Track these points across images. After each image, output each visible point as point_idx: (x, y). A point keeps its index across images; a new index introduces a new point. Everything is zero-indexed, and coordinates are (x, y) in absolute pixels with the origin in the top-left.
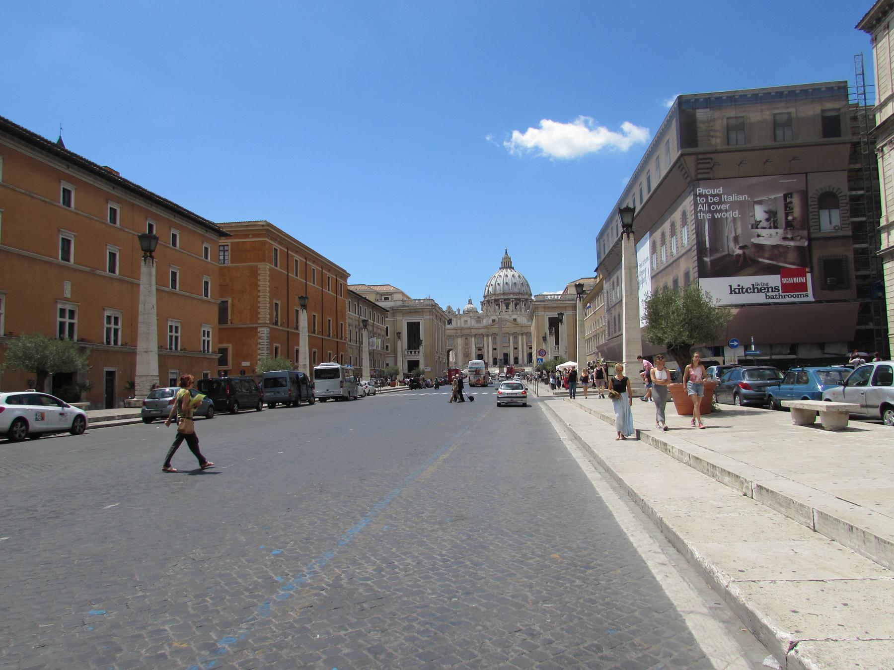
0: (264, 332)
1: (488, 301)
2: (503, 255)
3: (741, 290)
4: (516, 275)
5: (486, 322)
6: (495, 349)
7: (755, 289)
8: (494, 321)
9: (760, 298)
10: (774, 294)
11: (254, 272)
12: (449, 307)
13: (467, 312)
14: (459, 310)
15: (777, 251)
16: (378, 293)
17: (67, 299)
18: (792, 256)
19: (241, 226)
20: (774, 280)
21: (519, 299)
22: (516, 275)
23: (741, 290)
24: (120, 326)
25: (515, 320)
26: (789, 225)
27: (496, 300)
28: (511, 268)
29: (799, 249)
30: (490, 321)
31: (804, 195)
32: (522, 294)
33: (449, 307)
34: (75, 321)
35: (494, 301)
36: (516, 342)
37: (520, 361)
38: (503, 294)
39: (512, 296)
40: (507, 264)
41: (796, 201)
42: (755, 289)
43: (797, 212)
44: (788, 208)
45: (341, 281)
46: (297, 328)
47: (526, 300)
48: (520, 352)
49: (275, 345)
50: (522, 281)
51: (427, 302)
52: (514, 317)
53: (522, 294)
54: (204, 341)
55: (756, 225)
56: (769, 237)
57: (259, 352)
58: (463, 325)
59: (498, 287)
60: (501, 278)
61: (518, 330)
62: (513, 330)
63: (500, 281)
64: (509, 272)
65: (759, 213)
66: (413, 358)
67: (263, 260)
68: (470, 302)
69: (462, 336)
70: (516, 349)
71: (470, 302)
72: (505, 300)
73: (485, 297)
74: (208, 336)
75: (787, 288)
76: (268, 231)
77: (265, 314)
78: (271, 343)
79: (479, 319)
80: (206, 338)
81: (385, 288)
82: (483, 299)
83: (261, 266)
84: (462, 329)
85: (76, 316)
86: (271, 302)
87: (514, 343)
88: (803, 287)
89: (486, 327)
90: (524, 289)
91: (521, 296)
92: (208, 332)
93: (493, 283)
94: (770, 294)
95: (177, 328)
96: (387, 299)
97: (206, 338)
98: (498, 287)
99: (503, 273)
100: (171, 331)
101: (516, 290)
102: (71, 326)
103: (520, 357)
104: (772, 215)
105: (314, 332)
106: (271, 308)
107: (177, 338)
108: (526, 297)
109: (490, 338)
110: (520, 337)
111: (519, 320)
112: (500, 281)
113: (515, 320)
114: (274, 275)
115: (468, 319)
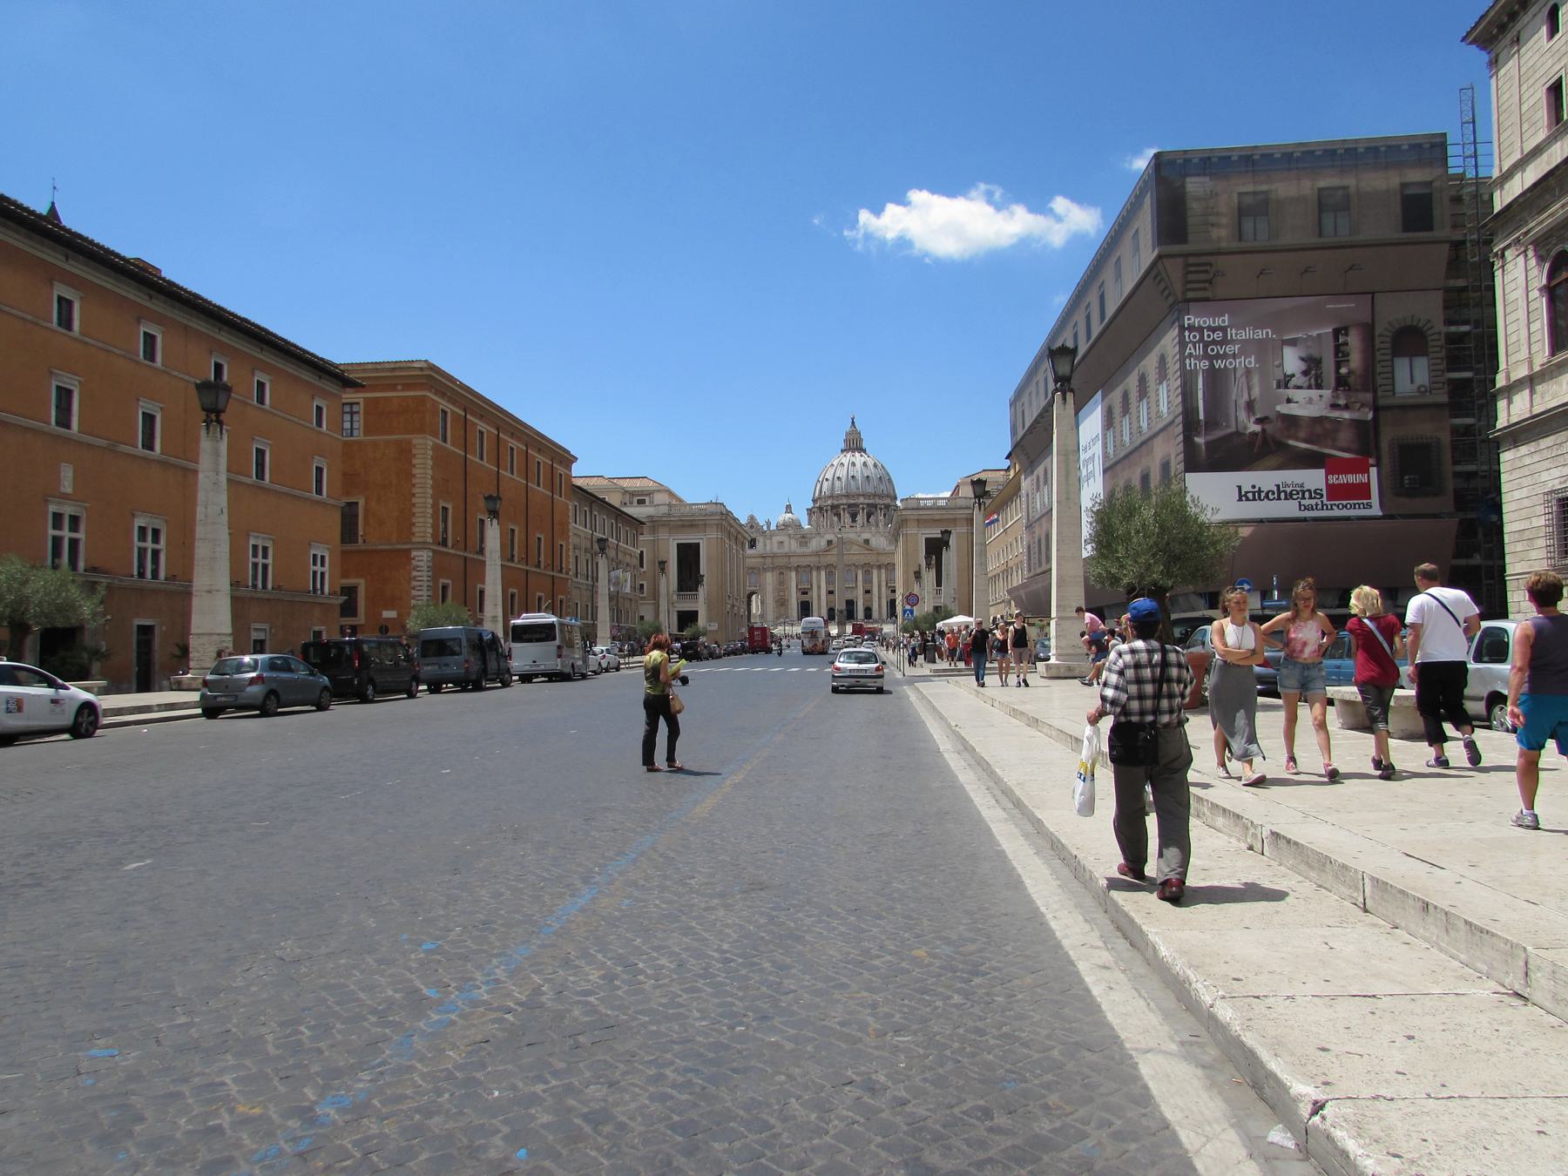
0: (422, 558)
1: (820, 509)
2: (848, 427)
3: (1257, 495)
4: (870, 463)
5: (817, 544)
6: (831, 592)
7: (1281, 493)
8: (829, 542)
9: (1289, 509)
10: (1313, 502)
11: (405, 453)
12: (752, 518)
13: (784, 527)
14: (769, 524)
15: (1320, 428)
16: (625, 492)
17: (65, 496)
18: (1345, 436)
19: (383, 370)
20: (1314, 478)
21: (875, 506)
22: (870, 463)
23: (1257, 495)
24: (270, 561)
25: (867, 542)
26: (1341, 382)
27: (833, 507)
28: (861, 450)
29: (1358, 424)
30: (824, 543)
31: (1368, 331)
32: (880, 497)
33: (752, 518)
34: (81, 535)
35: (830, 507)
36: (867, 580)
37: (875, 614)
38: (847, 496)
39: (862, 500)
40: (854, 444)
41: (1354, 341)
42: (1281, 493)
43: (1355, 360)
44: (1340, 353)
45: (560, 469)
46: (481, 551)
47: (887, 507)
48: (876, 599)
49: (442, 581)
50: (880, 473)
51: (713, 508)
52: (866, 536)
53: (880, 497)
54: (315, 573)
55: (1285, 382)
56: (1307, 403)
57: (414, 593)
58: (775, 550)
59: (837, 483)
60: (844, 467)
61: (871, 559)
62: (863, 560)
63: (842, 473)
64: (858, 458)
65: (1292, 361)
66: (687, 606)
67: (421, 430)
68: (789, 509)
69: (773, 569)
70: (868, 592)
71: (789, 509)
72: (850, 506)
73: (814, 501)
74: (323, 565)
75: (1335, 492)
76: (431, 378)
77: (424, 527)
78: (434, 578)
79: (804, 539)
80: (319, 568)
81: (638, 483)
82: (811, 505)
83: (417, 440)
84: (774, 556)
85: (82, 527)
86: (435, 505)
87: (865, 581)
88: (1362, 491)
89: (817, 554)
90: (882, 487)
91: (878, 501)
92: (323, 558)
93: (830, 476)
94: (1306, 502)
95: (265, 549)
96: (641, 502)
97: (319, 568)
98: (837, 483)
99: (847, 458)
100: (255, 555)
101: (870, 490)
102: (74, 543)
103: (875, 607)
104: (1312, 365)
105: (512, 559)
106: (435, 516)
107: (265, 567)
108: (888, 501)
109: (823, 573)
110: (875, 572)
111: (873, 542)
112: (842, 473)
113: (867, 542)
114: (440, 457)
115: (785, 539)
